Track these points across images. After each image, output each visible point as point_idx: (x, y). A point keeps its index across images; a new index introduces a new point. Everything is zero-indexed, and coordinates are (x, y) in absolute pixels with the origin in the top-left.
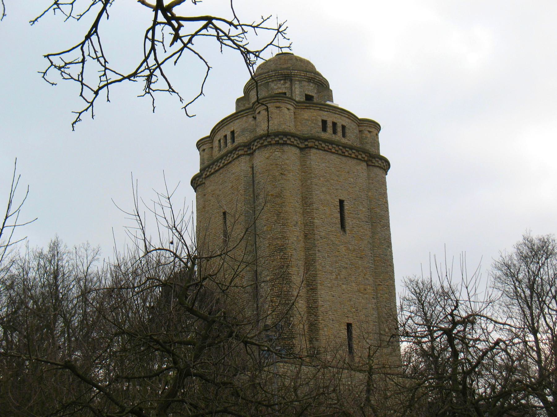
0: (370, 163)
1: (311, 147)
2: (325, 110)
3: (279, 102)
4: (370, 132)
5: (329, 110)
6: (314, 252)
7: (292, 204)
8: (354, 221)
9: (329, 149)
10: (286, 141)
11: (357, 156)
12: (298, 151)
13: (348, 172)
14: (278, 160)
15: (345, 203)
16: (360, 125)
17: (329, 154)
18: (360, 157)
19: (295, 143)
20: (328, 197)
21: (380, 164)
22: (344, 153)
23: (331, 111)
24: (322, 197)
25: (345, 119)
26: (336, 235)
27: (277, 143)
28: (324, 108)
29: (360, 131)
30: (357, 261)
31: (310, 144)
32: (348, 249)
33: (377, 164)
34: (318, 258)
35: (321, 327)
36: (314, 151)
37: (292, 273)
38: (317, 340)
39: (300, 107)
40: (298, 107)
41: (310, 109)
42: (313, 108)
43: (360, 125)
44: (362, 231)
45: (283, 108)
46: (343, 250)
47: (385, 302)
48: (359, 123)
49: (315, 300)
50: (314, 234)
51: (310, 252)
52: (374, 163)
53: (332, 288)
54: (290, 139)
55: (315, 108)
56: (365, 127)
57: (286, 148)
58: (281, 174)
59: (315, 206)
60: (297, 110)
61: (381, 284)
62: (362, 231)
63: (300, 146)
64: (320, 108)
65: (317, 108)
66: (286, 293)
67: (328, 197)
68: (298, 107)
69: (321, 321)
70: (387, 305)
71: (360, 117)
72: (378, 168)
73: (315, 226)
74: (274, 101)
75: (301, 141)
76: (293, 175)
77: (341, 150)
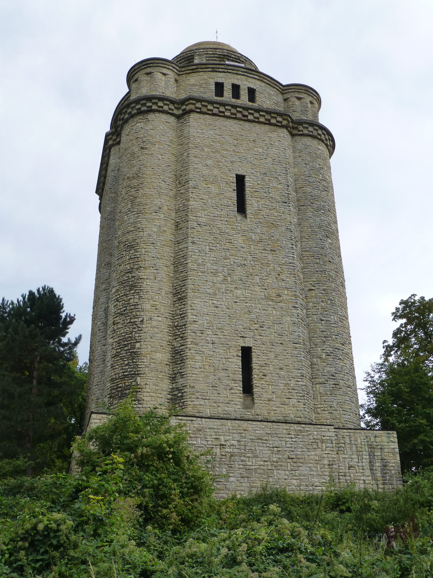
0: (295, 132)
1: (191, 111)
2: (220, 70)
3: (150, 67)
4: (299, 99)
5: (226, 71)
6: (185, 245)
7: (154, 184)
8: (262, 202)
9: (220, 112)
10: (151, 107)
11: (269, 120)
12: (172, 119)
13: (254, 141)
14: (140, 133)
15: (247, 179)
16: (284, 92)
17: (222, 119)
18: (273, 121)
19: (166, 108)
20: (216, 172)
21: (312, 132)
22: (247, 116)
23: (229, 71)
24: (206, 172)
25: (253, 81)
26: (227, 221)
27: (140, 112)
28: (219, 68)
29: (285, 100)
30: (266, 255)
31: (188, 108)
32: (249, 239)
33: (306, 132)
34: (190, 253)
35: (189, 354)
36: (193, 116)
37: (145, 277)
38: (182, 376)
39: (184, 72)
40: (182, 73)
41: (199, 72)
42: (202, 70)
43: (284, 92)
44: (276, 214)
45: (155, 73)
46: (240, 241)
47: (321, 314)
48: (283, 90)
49: (182, 314)
50: (188, 221)
51: (180, 247)
52: (302, 131)
53: (216, 294)
54: (156, 104)
55: (205, 70)
56: (292, 94)
57: (151, 116)
58: (142, 148)
59: (191, 183)
60: (181, 76)
61: (313, 288)
62: (276, 214)
63: (175, 112)
64: (213, 68)
65: (208, 70)
66: (133, 307)
67: (216, 172)
68: (182, 73)
69: (188, 346)
70: (323, 318)
71: (284, 83)
72: (309, 138)
73: (190, 210)
74: (143, 67)
75: (176, 105)
76: (159, 148)
77: (241, 112)
